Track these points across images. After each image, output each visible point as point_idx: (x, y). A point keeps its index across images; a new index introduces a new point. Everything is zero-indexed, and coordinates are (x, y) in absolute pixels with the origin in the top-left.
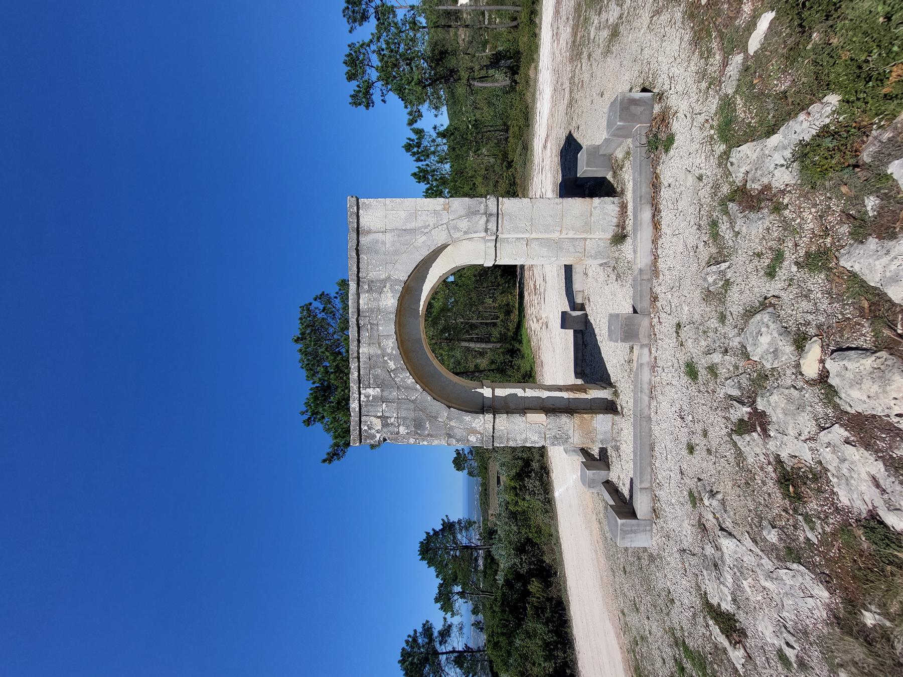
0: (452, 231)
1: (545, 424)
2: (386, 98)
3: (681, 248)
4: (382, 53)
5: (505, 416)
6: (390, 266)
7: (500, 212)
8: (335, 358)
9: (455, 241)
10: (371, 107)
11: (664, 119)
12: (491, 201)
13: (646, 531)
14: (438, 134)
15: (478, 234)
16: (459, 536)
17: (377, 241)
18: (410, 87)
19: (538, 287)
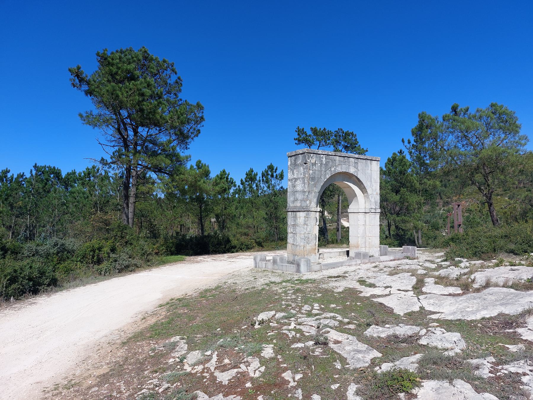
1: (313, 233)
17: (368, 167)
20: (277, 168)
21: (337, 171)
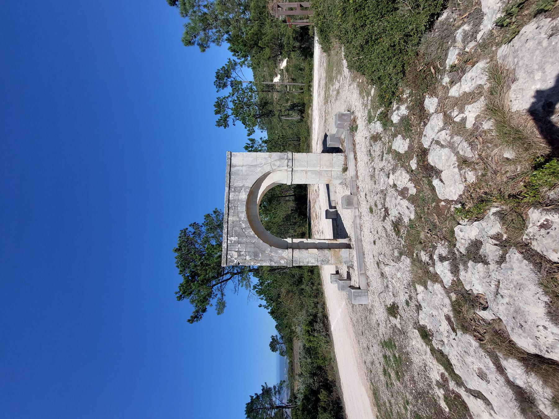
0: (272, 166)
1: (317, 254)
2: (235, 123)
3: (363, 165)
4: (235, 102)
5: (298, 250)
6: (244, 181)
7: (293, 158)
8: (201, 258)
9: (274, 171)
10: (227, 127)
11: (354, 120)
12: (290, 154)
13: (365, 295)
14: (262, 141)
15: (284, 167)
16: (274, 399)
17: (239, 170)
18: (249, 118)
19: (317, 214)
20: (246, 144)
21: (246, 219)
